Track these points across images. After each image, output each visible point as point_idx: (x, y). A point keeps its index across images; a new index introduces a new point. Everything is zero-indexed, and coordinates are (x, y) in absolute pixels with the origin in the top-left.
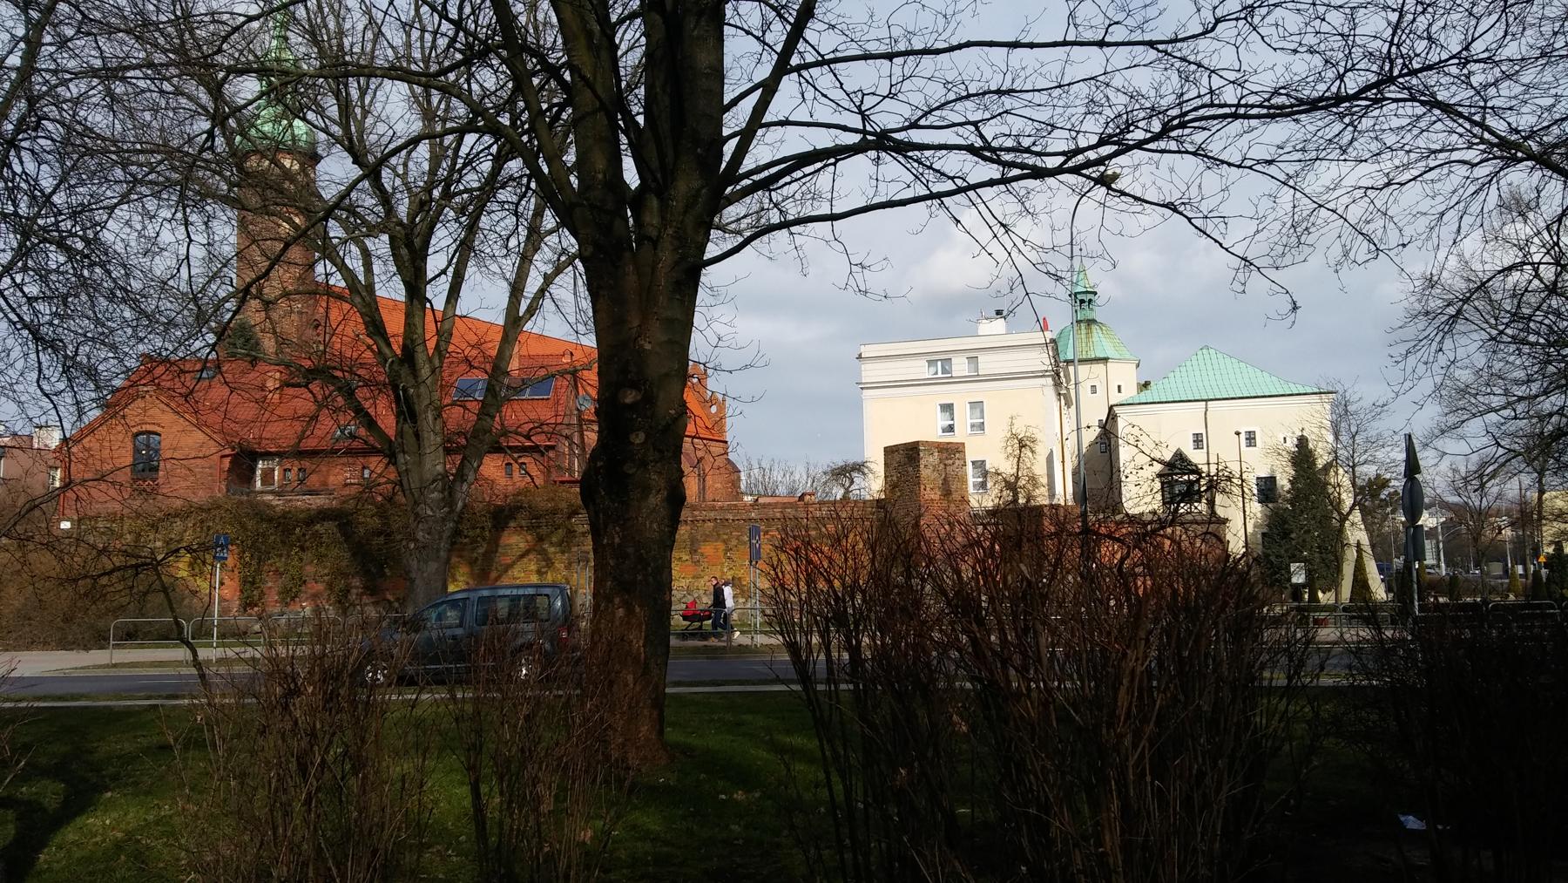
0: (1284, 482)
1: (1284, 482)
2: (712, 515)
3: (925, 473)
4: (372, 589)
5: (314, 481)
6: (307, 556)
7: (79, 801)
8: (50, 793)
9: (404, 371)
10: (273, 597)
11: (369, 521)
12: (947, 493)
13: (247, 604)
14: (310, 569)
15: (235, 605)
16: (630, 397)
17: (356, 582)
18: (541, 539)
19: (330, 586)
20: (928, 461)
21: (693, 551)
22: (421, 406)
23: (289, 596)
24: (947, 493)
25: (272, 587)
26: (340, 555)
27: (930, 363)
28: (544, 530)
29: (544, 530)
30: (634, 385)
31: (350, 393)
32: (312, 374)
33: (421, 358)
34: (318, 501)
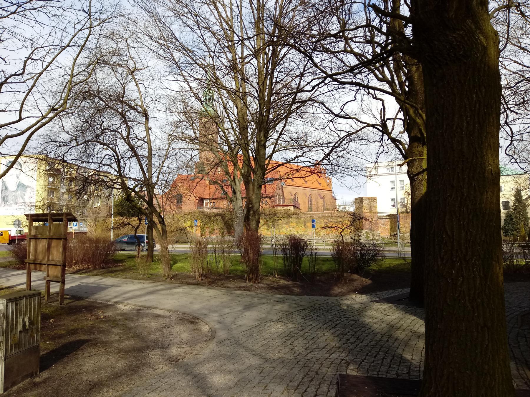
0: (511, 204)
1: (511, 204)
2: (310, 215)
3: (364, 205)
4: (229, 232)
5: (217, 205)
6: (215, 224)
7: (175, 263)
8: (172, 263)
9: (233, 183)
10: (207, 234)
11: (227, 216)
12: (371, 211)
13: (202, 235)
14: (216, 227)
15: (199, 235)
16: (250, 206)
17: (225, 230)
18: (267, 221)
19: (220, 231)
20: (366, 202)
21: (305, 225)
22: (237, 191)
23: (211, 233)
24: (371, 211)
25: (207, 231)
26: (221, 224)
27: (388, 169)
28: (268, 219)
29: (268, 219)
30: (251, 204)
31: (222, 187)
32: (215, 183)
33: (237, 180)
34: (215, 211)
